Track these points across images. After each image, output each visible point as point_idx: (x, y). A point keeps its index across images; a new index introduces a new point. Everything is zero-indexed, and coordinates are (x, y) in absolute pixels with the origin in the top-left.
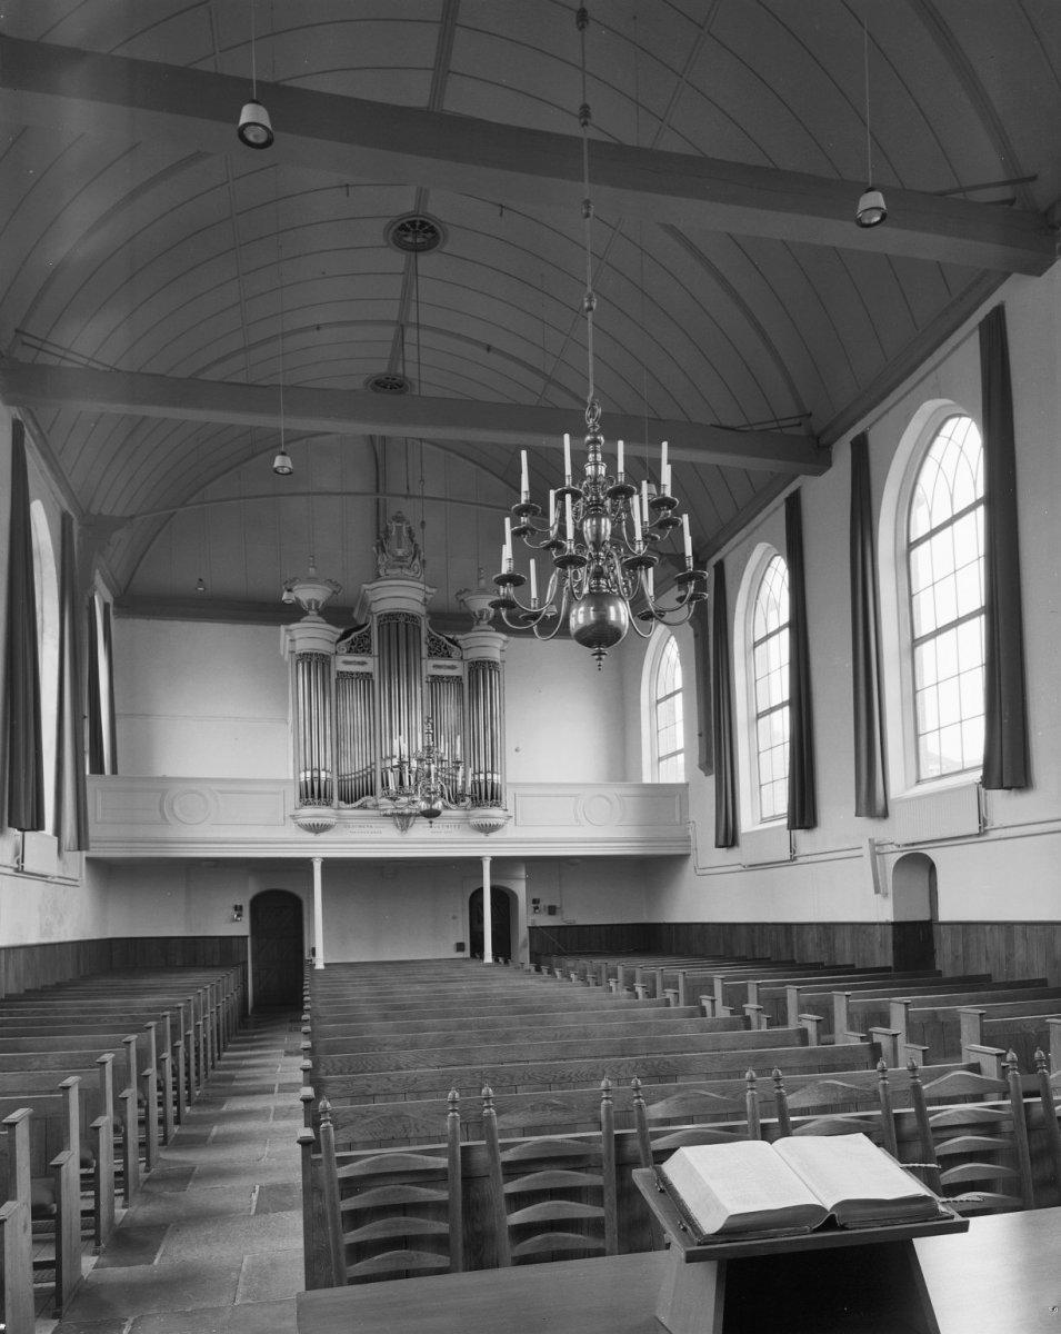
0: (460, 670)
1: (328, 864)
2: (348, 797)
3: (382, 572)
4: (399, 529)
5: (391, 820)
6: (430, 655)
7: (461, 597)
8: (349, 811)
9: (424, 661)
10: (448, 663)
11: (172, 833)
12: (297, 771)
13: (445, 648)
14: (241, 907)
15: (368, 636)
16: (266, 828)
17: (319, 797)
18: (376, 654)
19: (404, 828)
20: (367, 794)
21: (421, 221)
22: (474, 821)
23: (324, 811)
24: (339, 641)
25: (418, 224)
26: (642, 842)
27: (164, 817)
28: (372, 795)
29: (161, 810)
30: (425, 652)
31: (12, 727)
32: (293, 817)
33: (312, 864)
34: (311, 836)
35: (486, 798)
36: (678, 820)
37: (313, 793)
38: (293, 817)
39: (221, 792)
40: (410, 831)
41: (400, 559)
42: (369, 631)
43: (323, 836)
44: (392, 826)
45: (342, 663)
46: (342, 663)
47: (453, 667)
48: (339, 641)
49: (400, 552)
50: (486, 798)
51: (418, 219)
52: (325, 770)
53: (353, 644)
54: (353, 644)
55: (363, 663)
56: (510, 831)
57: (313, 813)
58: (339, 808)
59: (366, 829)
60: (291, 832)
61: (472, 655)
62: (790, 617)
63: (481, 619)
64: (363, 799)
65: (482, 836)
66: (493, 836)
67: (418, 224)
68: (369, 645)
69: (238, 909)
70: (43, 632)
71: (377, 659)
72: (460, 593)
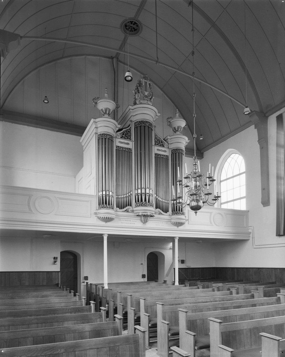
0: (168, 153)
1: (110, 237)
2: (121, 206)
3: (137, 102)
4: (146, 83)
5: (139, 218)
6: (156, 144)
7: (169, 120)
8: (121, 212)
9: (153, 147)
10: (163, 149)
11: (34, 218)
12: (98, 191)
13: (162, 142)
14: (57, 258)
15: (129, 131)
16: (84, 218)
17: (106, 203)
18: (134, 140)
19: (145, 222)
20: (128, 205)
21: (135, 22)
22: (173, 221)
23: (110, 211)
24: (117, 131)
25: (133, 23)
26: (233, 233)
27: (30, 210)
28: (130, 206)
29: (29, 206)
30: (153, 143)
31: (30, 222)
32: (96, 213)
33: (103, 238)
34: (103, 223)
35: (179, 210)
36: (245, 225)
37: (104, 203)
38: (96, 213)
39: (61, 199)
40: (147, 224)
41: (146, 96)
42: (130, 129)
43: (109, 224)
44: (139, 221)
45: (119, 142)
46: (119, 142)
47: (165, 151)
48: (117, 131)
49: (146, 93)
50: (179, 210)
51: (134, 21)
52: (112, 191)
53: (123, 134)
54: (123, 134)
55: (128, 144)
56: (186, 226)
57: (105, 212)
58: (116, 211)
59: (128, 222)
60: (94, 221)
61: (173, 146)
62: (246, 169)
63: (178, 131)
64: (128, 207)
65: (176, 228)
66: (180, 228)
67: (133, 23)
68: (130, 136)
69: (55, 258)
70: (83, 265)
71: (134, 143)
72: (168, 118)
